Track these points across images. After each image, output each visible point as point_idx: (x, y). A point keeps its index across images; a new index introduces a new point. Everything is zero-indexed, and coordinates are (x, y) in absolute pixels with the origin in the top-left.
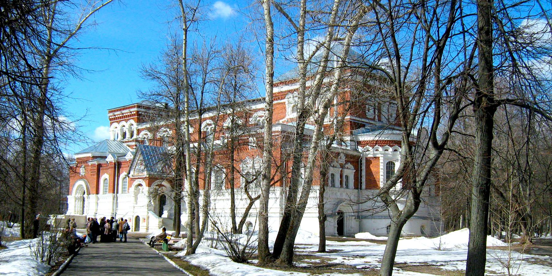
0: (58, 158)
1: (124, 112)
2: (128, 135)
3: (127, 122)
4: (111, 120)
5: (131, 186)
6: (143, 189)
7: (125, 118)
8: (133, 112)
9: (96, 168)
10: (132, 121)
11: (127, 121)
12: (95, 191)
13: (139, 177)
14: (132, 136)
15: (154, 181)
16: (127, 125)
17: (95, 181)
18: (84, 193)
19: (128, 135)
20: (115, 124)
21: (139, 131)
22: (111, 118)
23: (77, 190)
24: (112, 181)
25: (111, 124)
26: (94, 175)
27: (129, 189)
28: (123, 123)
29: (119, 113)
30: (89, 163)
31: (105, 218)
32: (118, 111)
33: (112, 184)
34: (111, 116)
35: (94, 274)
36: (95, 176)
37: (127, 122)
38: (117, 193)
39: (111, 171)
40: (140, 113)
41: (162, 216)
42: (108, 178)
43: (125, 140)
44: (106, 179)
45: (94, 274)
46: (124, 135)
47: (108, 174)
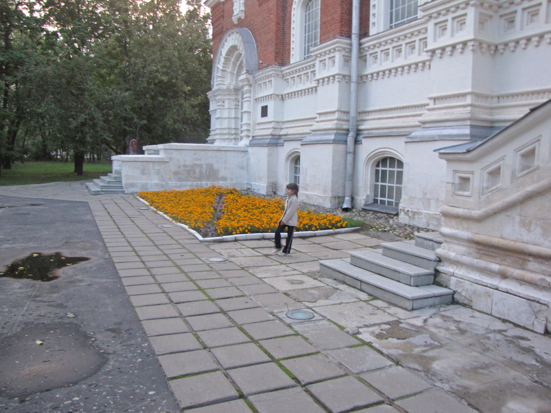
23: (227, 59)
38: (364, 32)
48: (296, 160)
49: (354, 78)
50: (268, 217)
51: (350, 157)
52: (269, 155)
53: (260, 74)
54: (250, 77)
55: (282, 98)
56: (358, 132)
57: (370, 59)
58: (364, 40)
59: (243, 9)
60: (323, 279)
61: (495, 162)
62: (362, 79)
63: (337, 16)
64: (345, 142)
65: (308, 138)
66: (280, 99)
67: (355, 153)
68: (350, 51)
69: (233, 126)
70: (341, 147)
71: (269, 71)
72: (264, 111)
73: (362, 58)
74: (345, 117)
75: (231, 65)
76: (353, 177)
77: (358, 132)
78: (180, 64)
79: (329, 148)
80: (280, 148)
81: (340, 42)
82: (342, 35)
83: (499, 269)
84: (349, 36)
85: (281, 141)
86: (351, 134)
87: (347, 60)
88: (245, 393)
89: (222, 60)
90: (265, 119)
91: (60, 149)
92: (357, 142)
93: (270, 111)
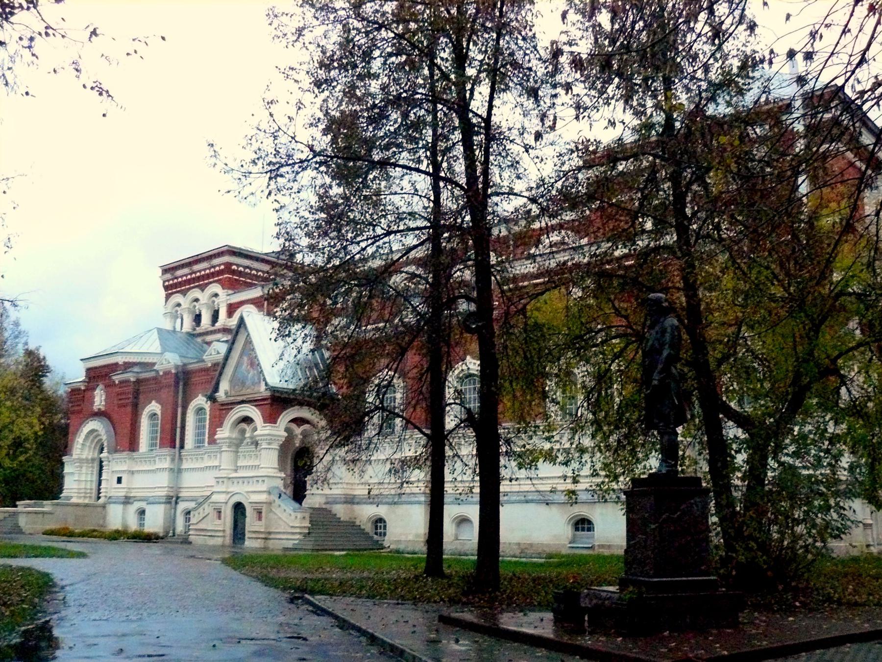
1: (196, 267)
2: (206, 319)
3: (203, 290)
4: (166, 288)
5: (221, 425)
6: (255, 429)
7: (201, 282)
8: (219, 265)
9: (130, 389)
10: (216, 288)
11: (202, 288)
12: (127, 445)
13: (244, 398)
14: (215, 317)
15: (285, 409)
16: (204, 296)
19: (206, 319)
20: (177, 298)
21: (232, 309)
22: (167, 283)
23: (87, 436)
28: (196, 293)
29: (186, 271)
30: (114, 378)
32: (183, 266)
33: (168, 426)
34: (168, 281)
36: (129, 409)
37: (203, 290)
38: (182, 447)
40: (234, 267)
41: (307, 503)
42: (159, 412)
43: (199, 330)
44: (155, 414)
46: (198, 318)
47: (158, 402)
48: (142, 512)
52: (124, 509)
53: (117, 455)
54: (110, 456)
55: (132, 473)
56: (178, 498)
57: (184, 461)
59: (103, 403)
60: (256, 648)
62: (180, 471)
63: (169, 437)
65: (151, 500)
67: (175, 509)
69: (89, 487)
70: (168, 506)
71: (125, 454)
72: (119, 480)
73: (180, 459)
75: (87, 449)
76: (174, 520)
77: (178, 498)
78: (9, 356)
79: (162, 507)
80: (129, 506)
81: (167, 451)
83: (136, 531)
84: (174, 447)
85: (131, 501)
86: (174, 499)
87: (173, 460)
89: (79, 446)
90: (119, 486)
92: (176, 503)
93: (123, 480)
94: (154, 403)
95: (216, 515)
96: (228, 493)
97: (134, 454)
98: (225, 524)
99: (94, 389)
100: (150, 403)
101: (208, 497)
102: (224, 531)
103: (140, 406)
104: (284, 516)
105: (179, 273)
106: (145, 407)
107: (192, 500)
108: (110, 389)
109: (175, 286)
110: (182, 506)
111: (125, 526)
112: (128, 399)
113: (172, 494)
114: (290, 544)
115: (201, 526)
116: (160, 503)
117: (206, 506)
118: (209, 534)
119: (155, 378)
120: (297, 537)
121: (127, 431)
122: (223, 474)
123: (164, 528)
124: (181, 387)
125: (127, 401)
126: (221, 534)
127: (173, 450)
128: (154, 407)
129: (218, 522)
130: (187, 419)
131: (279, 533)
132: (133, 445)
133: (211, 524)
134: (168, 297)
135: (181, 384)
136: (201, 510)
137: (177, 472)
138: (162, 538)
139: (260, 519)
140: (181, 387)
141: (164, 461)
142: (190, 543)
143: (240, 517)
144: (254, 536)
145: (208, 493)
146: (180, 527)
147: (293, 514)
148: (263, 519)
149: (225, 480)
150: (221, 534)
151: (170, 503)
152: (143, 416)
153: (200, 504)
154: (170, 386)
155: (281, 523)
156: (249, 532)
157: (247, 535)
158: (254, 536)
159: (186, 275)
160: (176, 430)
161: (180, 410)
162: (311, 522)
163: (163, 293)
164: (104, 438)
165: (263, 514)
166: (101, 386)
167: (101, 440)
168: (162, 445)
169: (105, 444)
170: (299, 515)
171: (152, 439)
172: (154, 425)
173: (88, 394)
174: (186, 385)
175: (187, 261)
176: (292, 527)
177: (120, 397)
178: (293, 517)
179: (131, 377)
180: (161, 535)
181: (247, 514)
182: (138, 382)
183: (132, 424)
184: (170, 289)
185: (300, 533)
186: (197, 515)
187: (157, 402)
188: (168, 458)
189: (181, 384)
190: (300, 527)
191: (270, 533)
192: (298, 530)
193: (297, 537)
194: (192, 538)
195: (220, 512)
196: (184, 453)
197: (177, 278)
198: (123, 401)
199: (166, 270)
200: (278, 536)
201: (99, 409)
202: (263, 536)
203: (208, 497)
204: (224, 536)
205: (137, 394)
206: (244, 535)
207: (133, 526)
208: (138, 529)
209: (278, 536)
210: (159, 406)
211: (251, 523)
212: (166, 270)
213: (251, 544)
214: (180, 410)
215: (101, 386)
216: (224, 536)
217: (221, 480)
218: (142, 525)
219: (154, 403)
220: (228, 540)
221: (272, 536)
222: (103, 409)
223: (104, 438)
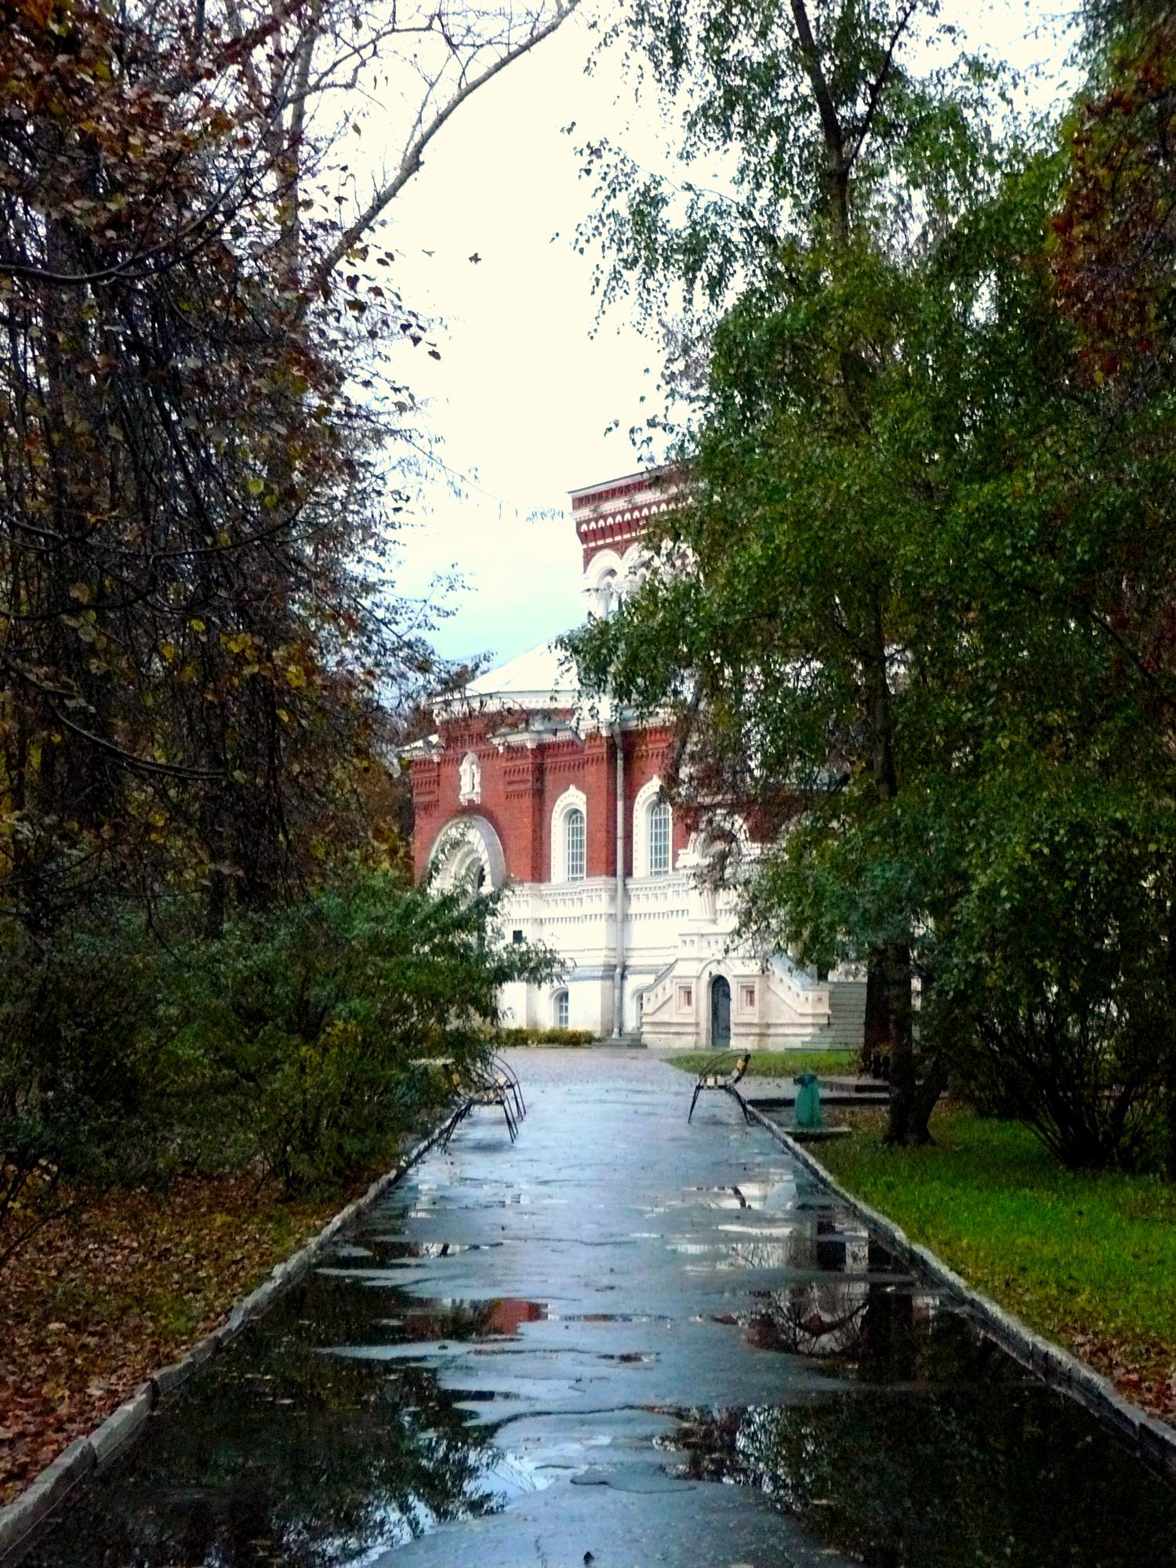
0: (305, 703)
4: (584, 537)
9: (527, 763)
12: (529, 869)
17: (527, 820)
18: (482, 879)
20: (606, 558)
22: (584, 528)
24: (602, 819)
25: (589, 556)
26: (520, 795)
27: (676, 856)
29: (619, 503)
31: (751, 1341)
33: (601, 836)
34: (588, 522)
35: (412, 137)
36: (527, 802)
38: (628, 872)
39: (596, 773)
42: (583, 809)
44: (576, 811)
45: (412, 137)
47: (580, 788)
49: (619, 918)
50: (651, 283)
51: (617, 992)
56: (625, 968)
58: (628, 881)
59: (478, 789)
61: (697, 1002)
62: (626, 918)
63: (603, 856)
64: (612, 978)
66: (685, 124)
67: (622, 988)
68: (616, 890)
70: (609, 983)
74: (612, 954)
77: (625, 968)
79: (598, 984)
81: (600, 882)
82: (607, 874)
83: (552, 1031)
84: (614, 874)
86: (618, 970)
87: (613, 898)
88: (551, 686)
91: (947, 129)
92: (623, 977)
94: (572, 788)
95: (683, 998)
96: (701, 960)
97: (542, 887)
98: (697, 1014)
99: (459, 762)
100: (566, 789)
101: (671, 966)
102: (697, 1024)
103: (547, 795)
104: (788, 997)
105: (608, 507)
106: (557, 797)
107: (648, 972)
108: (486, 762)
109: (603, 533)
110: (633, 983)
111: (533, 1022)
112: (523, 781)
113: (613, 961)
114: (796, 1043)
115: (662, 1017)
116: (594, 978)
117: (667, 982)
118: (673, 1029)
119: (571, 743)
120: (810, 1030)
121: (526, 840)
122: (694, 928)
123: (603, 1024)
124: (620, 763)
125: (522, 787)
126: (691, 1029)
127: (611, 880)
128: (573, 798)
129: (687, 1009)
130: (635, 822)
131: (782, 1025)
132: (539, 871)
133: (678, 1013)
134: (589, 556)
135: (620, 755)
136: (659, 989)
137: (622, 920)
138: (599, 1040)
139: (752, 1002)
140: (620, 763)
141: (596, 895)
142: (645, 1046)
143: (722, 1000)
144: (742, 1030)
145: (671, 960)
146: (630, 1024)
147: (802, 993)
148: (756, 1003)
149: (695, 938)
150: (691, 1029)
151: (612, 978)
152: (555, 815)
153: (659, 980)
154: (596, 760)
155: (784, 1008)
156: (736, 1024)
157: (733, 1030)
158: (742, 1030)
159: (622, 513)
160: (615, 844)
161: (620, 804)
162: (831, 1006)
163: (579, 548)
164: (485, 857)
165: (756, 995)
166: (471, 756)
167: (471, 851)
168: (592, 872)
169: (487, 869)
170: (811, 995)
171: (574, 857)
172: (575, 832)
173: (446, 771)
174: (628, 759)
175: (623, 483)
176: (801, 1015)
177: (512, 778)
178: (802, 998)
179: (526, 740)
180: (597, 1035)
181: (733, 994)
182: (542, 749)
183: (534, 831)
184: (593, 538)
185: (813, 1025)
186: (653, 998)
187: (579, 788)
188: (605, 896)
189: (620, 755)
190: (814, 1015)
191: (768, 1026)
192: (809, 1020)
193: (810, 1030)
194: (647, 1038)
195: (689, 993)
196: (632, 884)
197: (604, 517)
198: (515, 787)
199: (580, 502)
200: (781, 1031)
201: (471, 801)
202: (756, 1030)
203: (671, 966)
204: (698, 1034)
205: (540, 771)
206: (729, 1030)
207: (548, 1022)
208: (557, 1027)
209: (781, 1031)
210: (584, 797)
211: (739, 1011)
212: (580, 502)
213: (737, 1043)
214: (620, 804)
215: (471, 756)
216: (698, 1034)
217: (688, 939)
218: (564, 1020)
219: (572, 788)
220: (704, 1039)
221: (772, 1031)
222: (478, 800)
223: (485, 857)
